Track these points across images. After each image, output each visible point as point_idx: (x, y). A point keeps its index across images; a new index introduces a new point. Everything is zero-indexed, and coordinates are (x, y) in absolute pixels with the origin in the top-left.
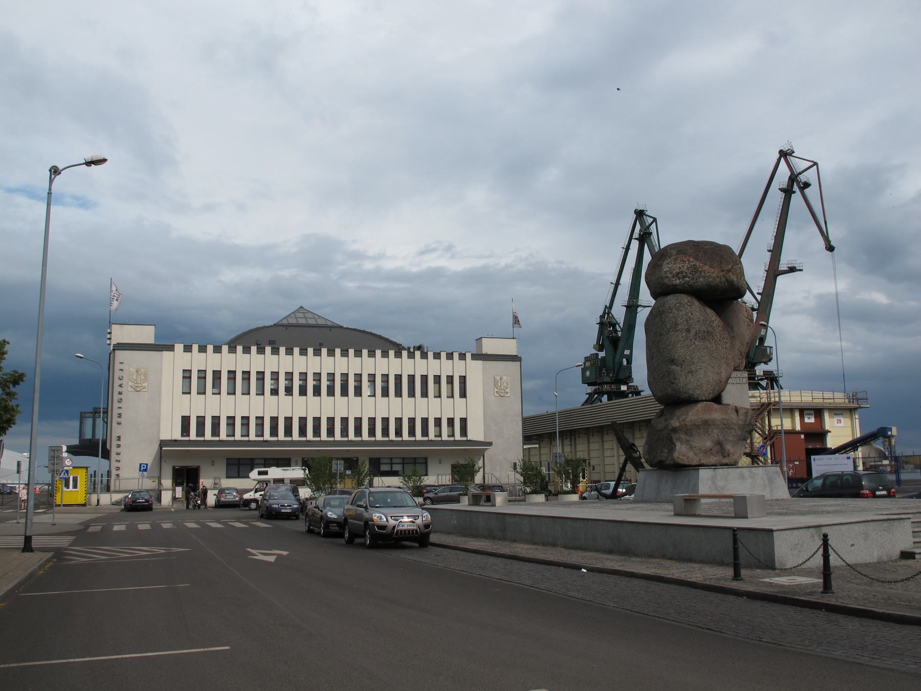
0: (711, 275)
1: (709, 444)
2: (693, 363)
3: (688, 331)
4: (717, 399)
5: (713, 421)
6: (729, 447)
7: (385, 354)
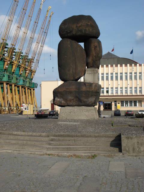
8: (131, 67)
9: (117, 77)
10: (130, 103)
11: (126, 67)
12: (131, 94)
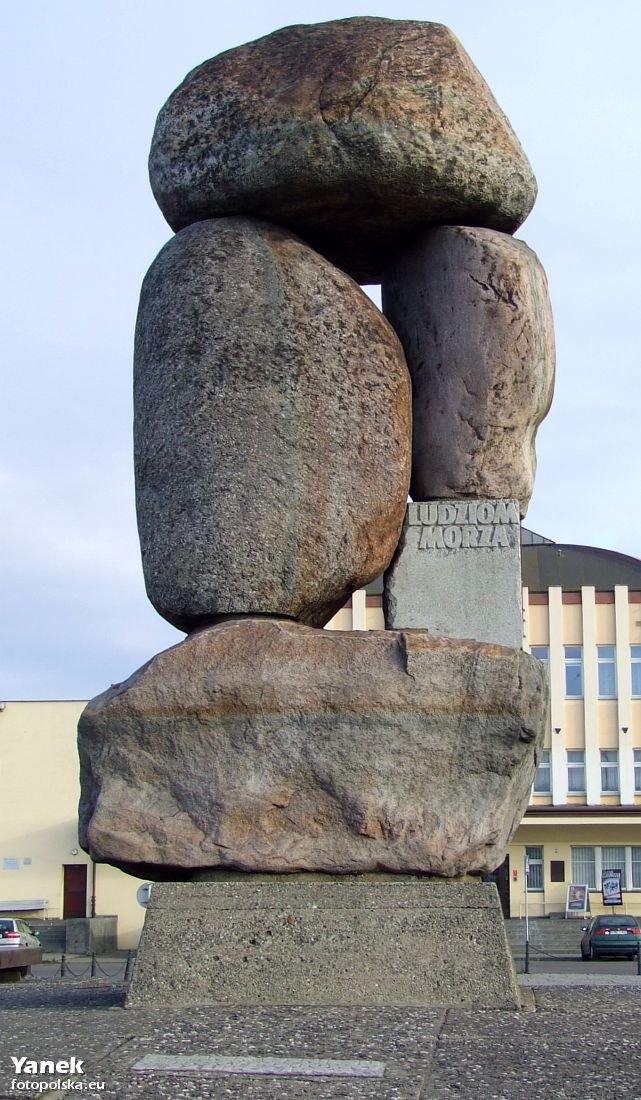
3: (195, 352)
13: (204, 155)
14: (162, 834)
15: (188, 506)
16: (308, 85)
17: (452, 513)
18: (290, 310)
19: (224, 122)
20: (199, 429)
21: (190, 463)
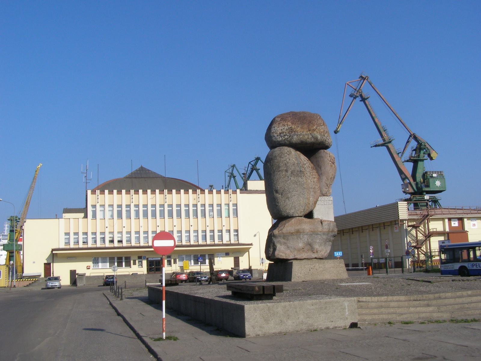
0: (303, 134)
1: (301, 245)
2: (290, 192)
3: (286, 171)
4: (310, 215)
5: (303, 229)
6: (316, 246)
7: (186, 192)
8: (227, 195)
9: (187, 212)
10: (125, 262)
11: (111, 195)
12: (188, 244)
13: (285, 135)
14: (286, 254)
15: (288, 198)
16: (305, 126)
17: (323, 199)
18: (301, 164)
19: (289, 130)
20: (289, 185)
21: (287, 190)
